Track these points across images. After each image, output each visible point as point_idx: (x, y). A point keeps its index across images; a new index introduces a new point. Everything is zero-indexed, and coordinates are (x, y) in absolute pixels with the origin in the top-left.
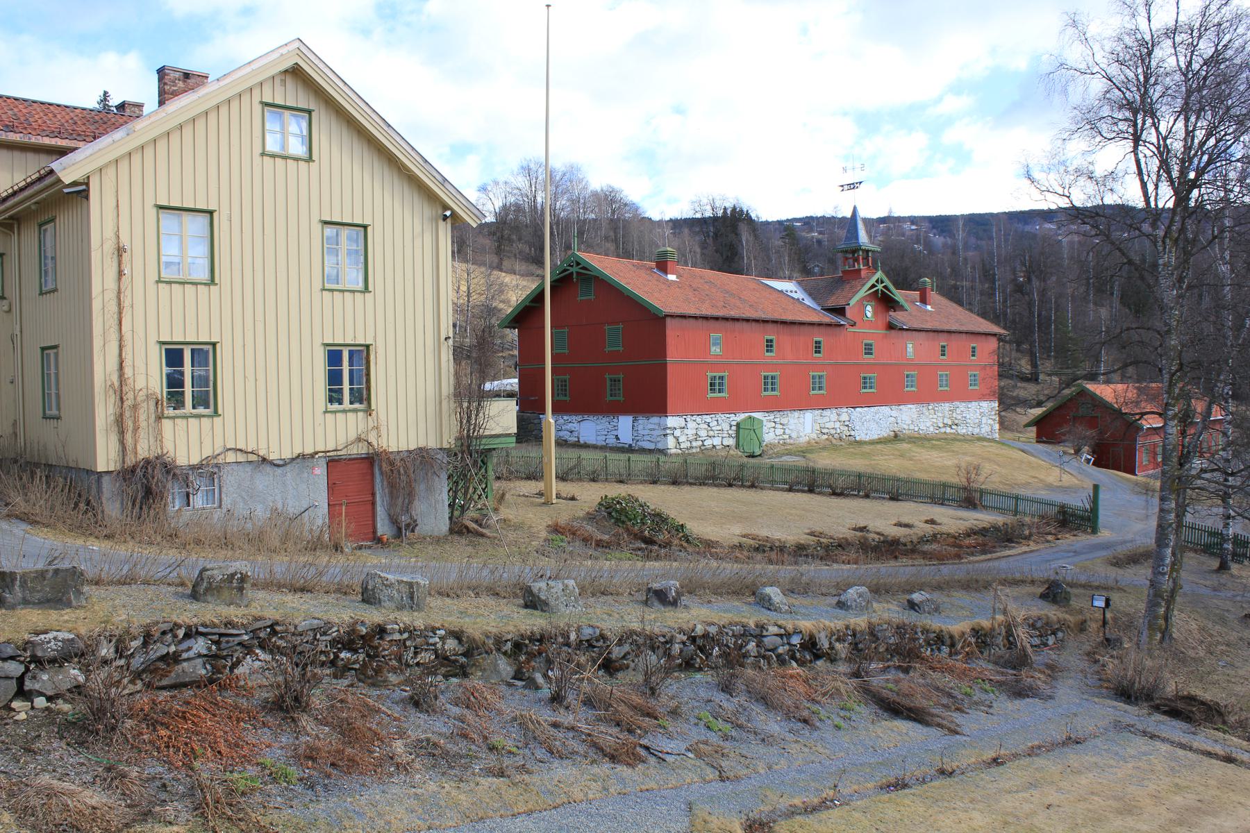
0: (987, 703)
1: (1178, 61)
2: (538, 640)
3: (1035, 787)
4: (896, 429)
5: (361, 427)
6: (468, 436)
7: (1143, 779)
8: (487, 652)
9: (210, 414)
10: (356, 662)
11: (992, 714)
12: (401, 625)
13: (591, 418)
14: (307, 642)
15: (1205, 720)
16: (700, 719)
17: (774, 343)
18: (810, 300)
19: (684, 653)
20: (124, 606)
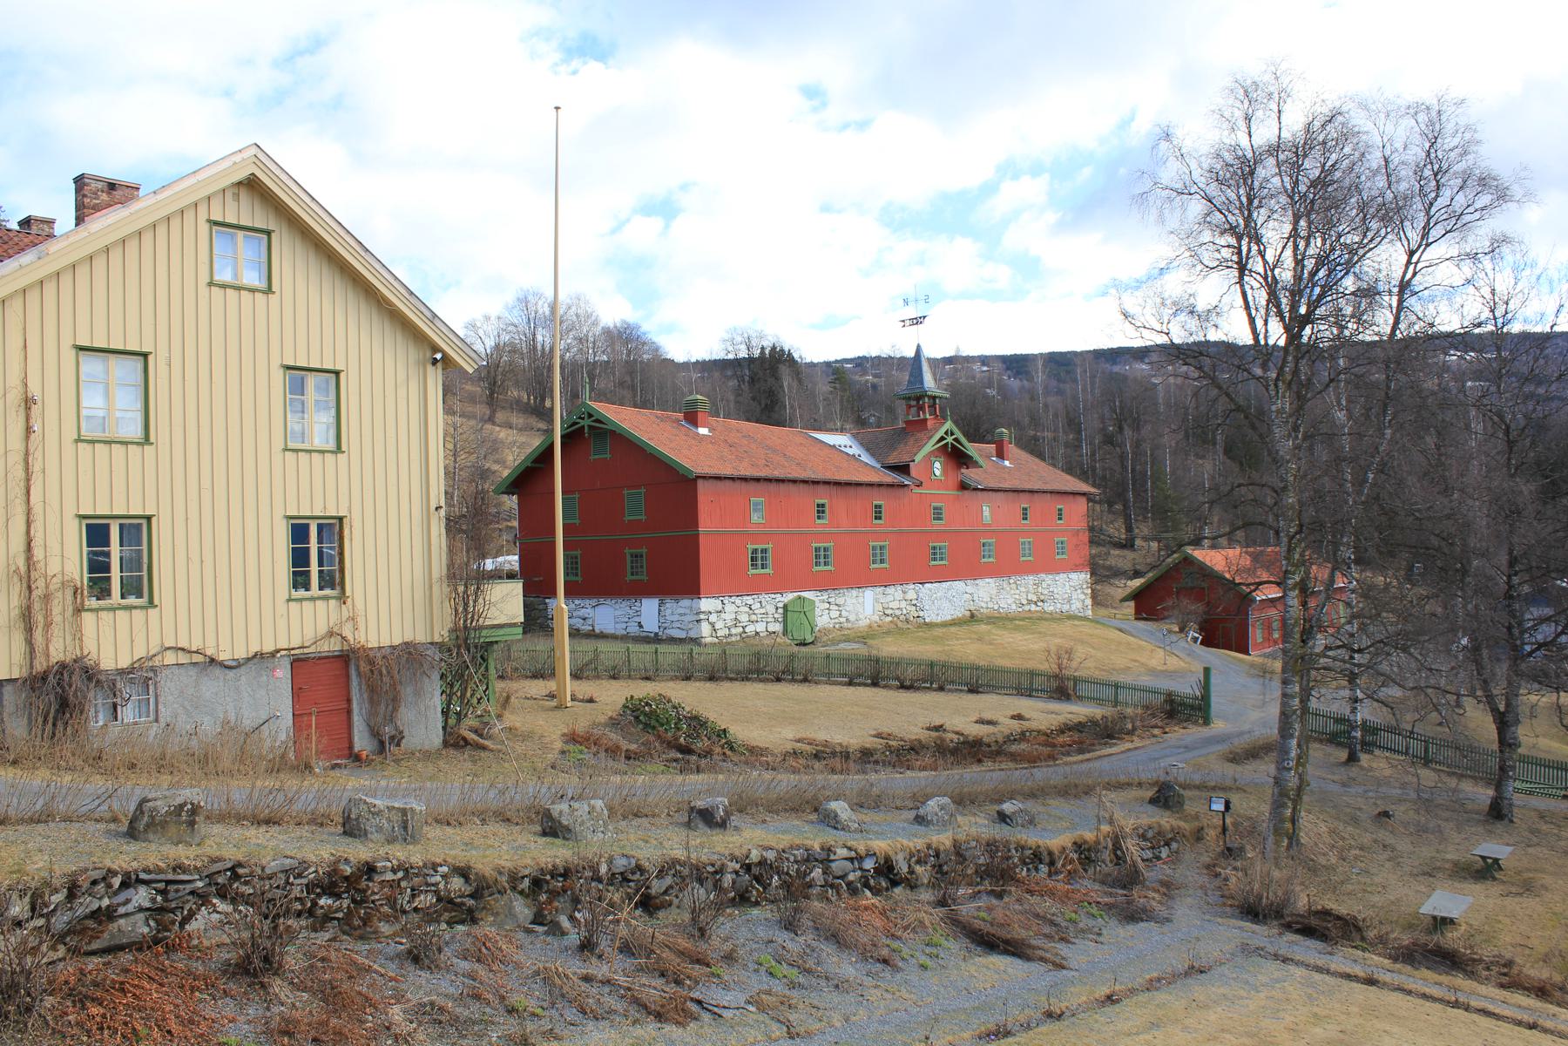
0: (1096, 930)
1: (1282, 181)
2: (561, 875)
3: (1158, 1026)
4: (972, 608)
5: (334, 618)
6: (466, 627)
7: (1278, 1011)
8: (499, 892)
9: (143, 604)
10: (339, 909)
11: (1102, 943)
12: (395, 862)
13: (608, 601)
14: (278, 887)
15: (1343, 937)
16: (761, 964)
17: (827, 509)
18: (869, 457)
19: (737, 885)
20: (41, 851)
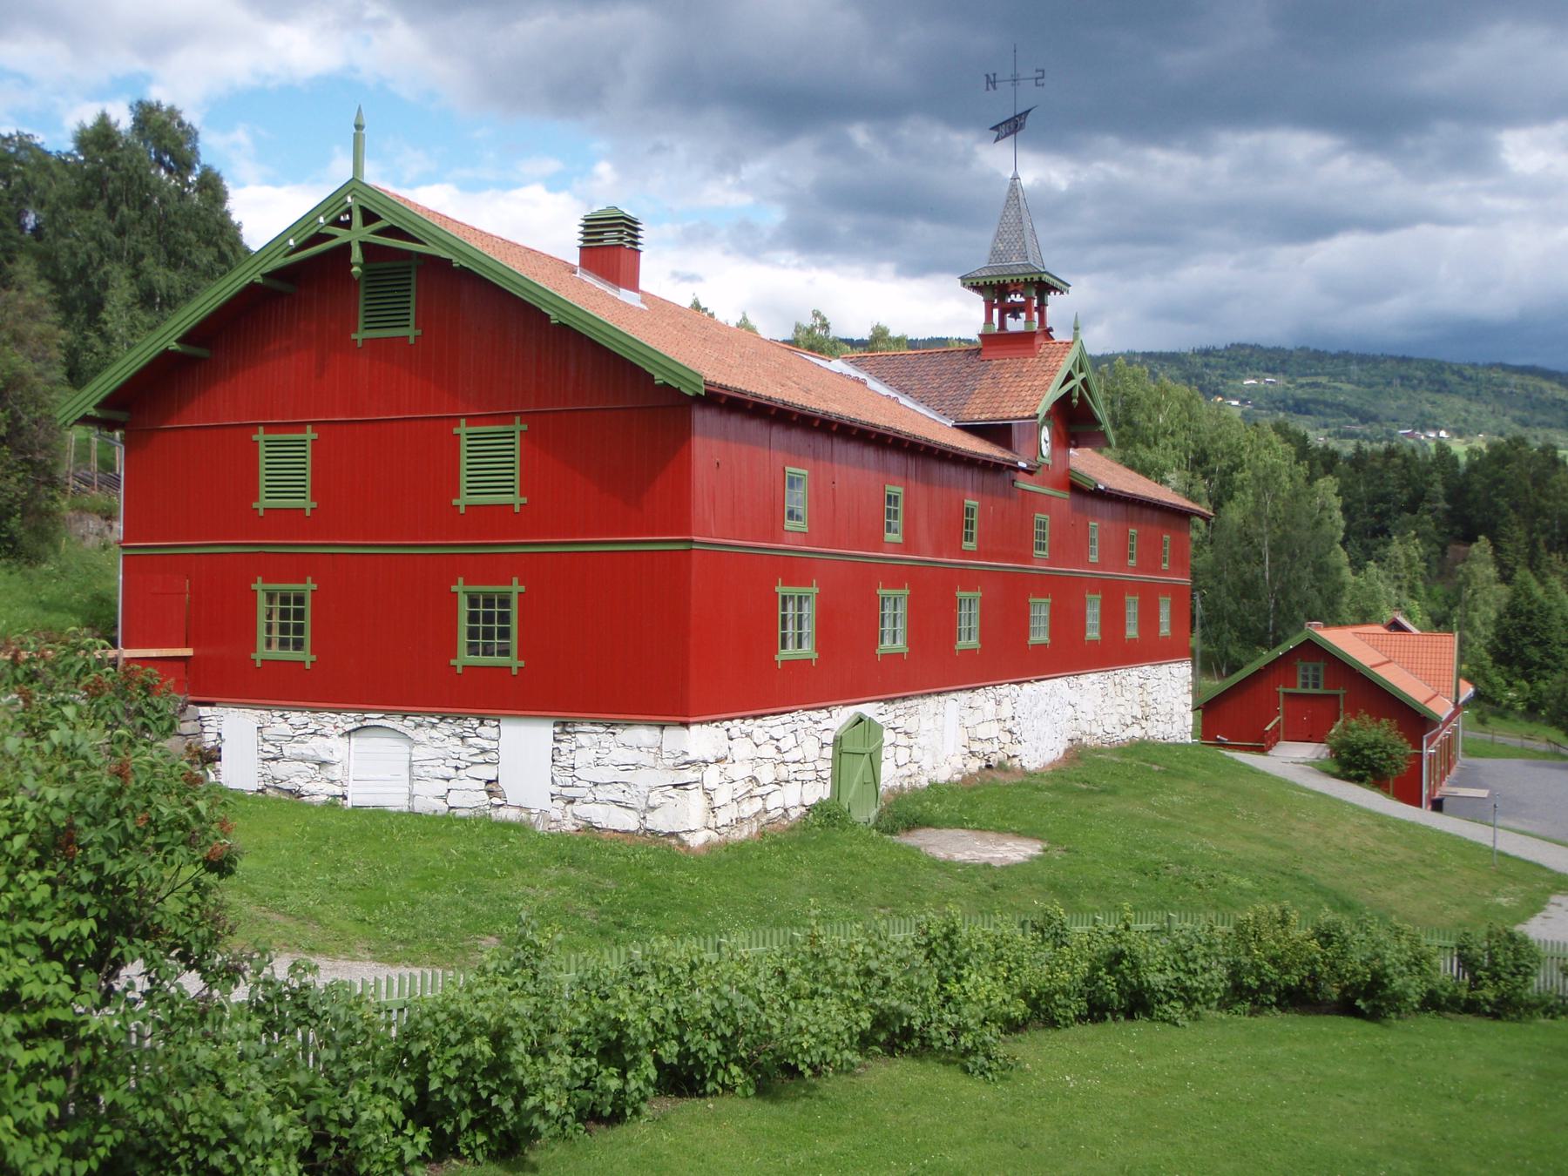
13: (394, 722)
